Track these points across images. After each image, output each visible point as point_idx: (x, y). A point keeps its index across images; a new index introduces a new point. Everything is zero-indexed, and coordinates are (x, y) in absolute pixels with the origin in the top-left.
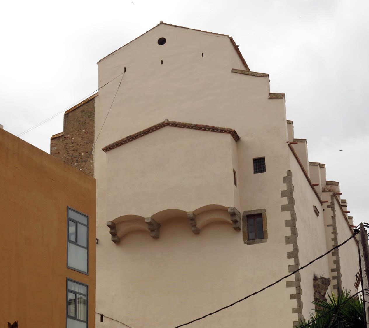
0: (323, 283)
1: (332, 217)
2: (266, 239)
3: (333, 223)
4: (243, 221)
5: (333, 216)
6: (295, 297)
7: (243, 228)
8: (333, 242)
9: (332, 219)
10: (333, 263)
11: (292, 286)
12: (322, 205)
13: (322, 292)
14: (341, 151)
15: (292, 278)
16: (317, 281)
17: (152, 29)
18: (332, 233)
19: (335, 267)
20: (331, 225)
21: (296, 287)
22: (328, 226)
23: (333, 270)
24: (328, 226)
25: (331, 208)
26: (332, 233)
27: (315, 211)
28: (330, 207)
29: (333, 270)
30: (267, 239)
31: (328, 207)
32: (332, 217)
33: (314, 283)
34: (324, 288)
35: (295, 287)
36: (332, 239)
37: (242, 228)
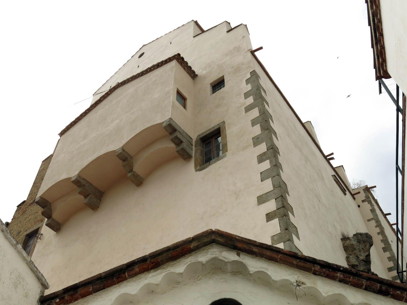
0: (359, 242)
1: (371, 210)
2: (225, 153)
3: (374, 216)
4: (196, 146)
5: (371, 209)
6: (271, 198)
7: (195, 155)
8: (380, 236)
9: (371, 212)
10: (388, 261)
11: (269, 200)
12: (354, 199)
13: (361, 255)
14: (349, 96)
15: (268, 185)
16: (348, 241)
17: (136, 53)
18: (376, 227)
19: (391, 264)
20: (372, 219)
21: (276, 199)
22: (368, 220)
23: (390, 269)
24: (368, 220)
25: (367, 202)
26: (376, 227)
27: (335, 180)
28: (366, 201)
29: (390, 269)
30: (227, 153)
31: (363, 201)
32: (371, 210)
33: (343, 244)
34: (362, 249)
35: (274, 200)
36: (378, 234)
37: (193, 155)
